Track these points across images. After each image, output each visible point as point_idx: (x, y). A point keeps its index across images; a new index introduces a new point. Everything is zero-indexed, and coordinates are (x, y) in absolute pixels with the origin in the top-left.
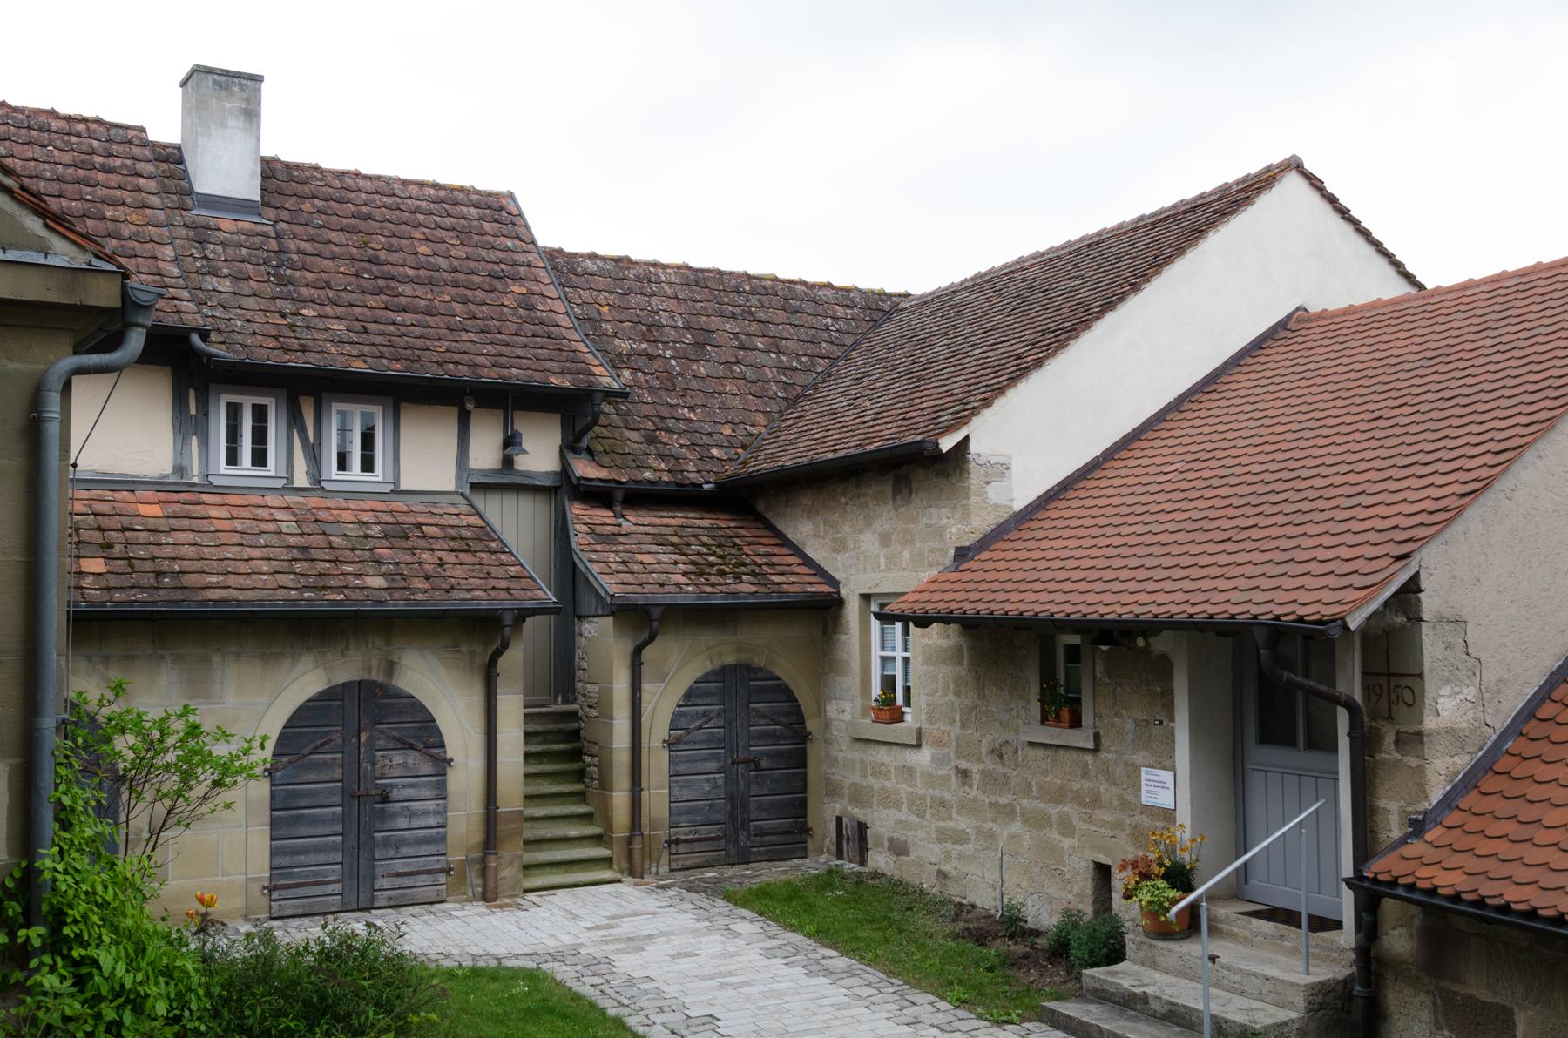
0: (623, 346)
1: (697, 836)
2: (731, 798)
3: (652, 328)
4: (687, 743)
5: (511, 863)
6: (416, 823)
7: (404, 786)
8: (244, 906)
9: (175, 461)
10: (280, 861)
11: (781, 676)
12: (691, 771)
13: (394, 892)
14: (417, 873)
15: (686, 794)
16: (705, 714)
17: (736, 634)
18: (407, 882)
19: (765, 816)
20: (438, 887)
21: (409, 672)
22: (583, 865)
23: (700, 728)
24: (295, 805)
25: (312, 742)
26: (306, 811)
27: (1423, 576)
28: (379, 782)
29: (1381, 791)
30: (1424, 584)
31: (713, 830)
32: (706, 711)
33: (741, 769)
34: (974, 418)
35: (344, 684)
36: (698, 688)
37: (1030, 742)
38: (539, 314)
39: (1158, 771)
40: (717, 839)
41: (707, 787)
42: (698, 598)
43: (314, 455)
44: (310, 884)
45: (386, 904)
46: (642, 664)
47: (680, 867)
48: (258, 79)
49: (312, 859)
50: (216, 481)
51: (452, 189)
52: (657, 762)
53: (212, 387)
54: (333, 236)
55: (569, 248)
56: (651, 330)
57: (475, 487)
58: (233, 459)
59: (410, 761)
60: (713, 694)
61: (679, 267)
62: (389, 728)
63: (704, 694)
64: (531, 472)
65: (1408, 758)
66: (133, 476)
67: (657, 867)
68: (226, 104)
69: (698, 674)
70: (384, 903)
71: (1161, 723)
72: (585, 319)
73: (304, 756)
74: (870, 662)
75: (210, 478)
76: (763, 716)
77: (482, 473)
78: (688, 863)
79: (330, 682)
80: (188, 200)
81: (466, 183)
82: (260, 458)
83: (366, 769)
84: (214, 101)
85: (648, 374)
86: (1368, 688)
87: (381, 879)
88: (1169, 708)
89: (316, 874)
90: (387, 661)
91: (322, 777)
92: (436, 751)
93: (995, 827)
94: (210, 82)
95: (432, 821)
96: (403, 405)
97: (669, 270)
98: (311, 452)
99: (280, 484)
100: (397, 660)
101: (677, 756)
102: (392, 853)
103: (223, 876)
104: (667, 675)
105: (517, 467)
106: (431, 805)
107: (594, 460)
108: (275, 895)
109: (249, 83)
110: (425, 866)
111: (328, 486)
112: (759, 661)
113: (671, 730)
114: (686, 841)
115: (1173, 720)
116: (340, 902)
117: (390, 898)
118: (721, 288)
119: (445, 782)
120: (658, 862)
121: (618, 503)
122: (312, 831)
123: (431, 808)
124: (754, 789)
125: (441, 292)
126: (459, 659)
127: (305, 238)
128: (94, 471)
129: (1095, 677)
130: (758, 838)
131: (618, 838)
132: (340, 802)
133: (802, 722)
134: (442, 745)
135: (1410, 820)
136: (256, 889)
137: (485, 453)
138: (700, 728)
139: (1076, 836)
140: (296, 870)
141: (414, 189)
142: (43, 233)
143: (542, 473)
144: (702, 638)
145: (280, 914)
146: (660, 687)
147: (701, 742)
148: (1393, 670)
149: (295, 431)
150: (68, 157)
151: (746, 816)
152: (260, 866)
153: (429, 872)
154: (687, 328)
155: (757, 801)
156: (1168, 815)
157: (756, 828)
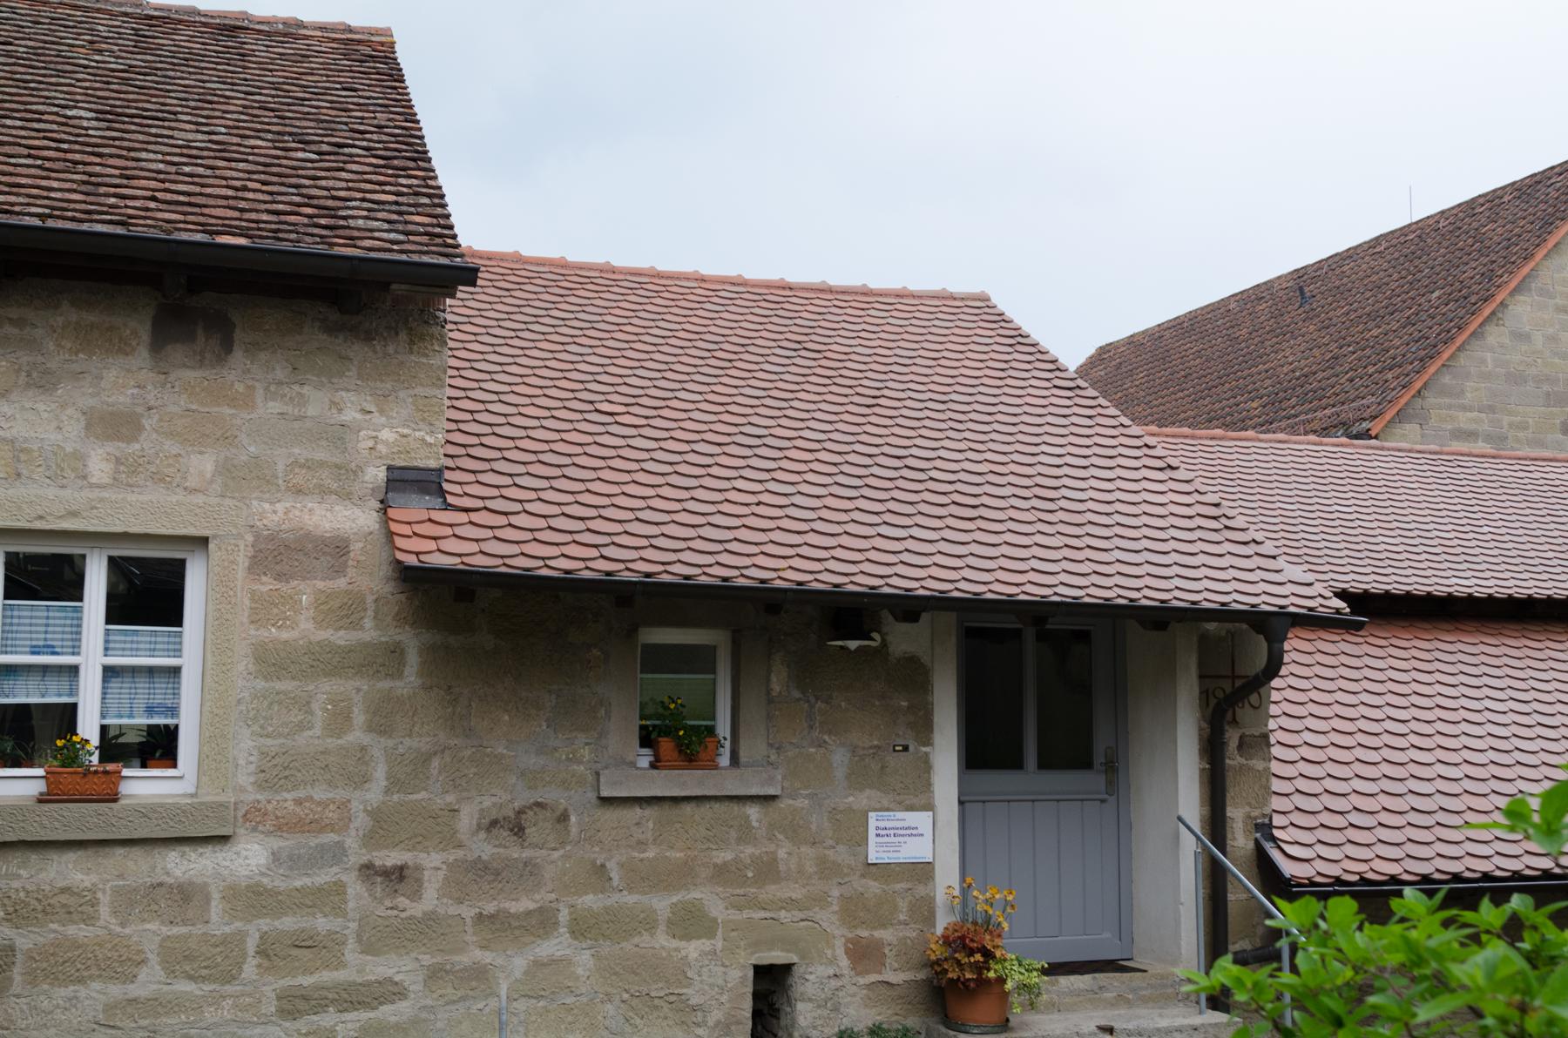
29: (1229, 801)
39: (900, 815)
65: (1254, 762)
71: (906, 748)
86: (1207, 691)
88: (924, 728)
93: (487, 957)
115: (928, 742)
129: (769, 692)
135: (1256, 825)
139: (719, 933)
148: (1238, 672)
156: (923, 872)
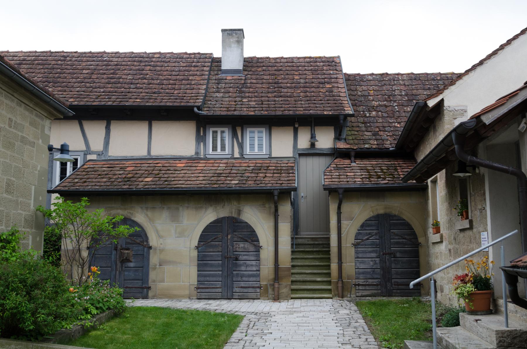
0: (375, 103)
1: (367, 283)
2: (382, 268)
3: (391, 96)
4: (362, 245)
5: (286, 287)
6: (248, 269)
7: (244, 255)
8: (189, 293)
9: (196, 151)
10: (202, 279)
11: (405, 219)
12: (364, 256)
13: (240, 293)
14: (249, 287)
15: (362, 266)
16: (370, 234)
17: (384, 202)
18: (245, 290)
19: (399, 277)
20: (257, 293)
21: (246, 214)
22: (320, 292)
23: (368, 239)
24: (205, 259)
25: (211, 238)
26: (209, 262)
28: (234, 253)
31: (375, 281)
32: (370, 232)
33: (387, 257)
34: (445, 91)
35: (222, 218)
36: (367, 223)
38: (334, 93)
40: (377, 285)
41: (371, 263)
42: (360, 185)
43: (241, 146)
44: (208, 288)
45: (237, 298)
46: (341, 213)
47: (360, 295)
48: (242, 30)
49: (211, 279)
50: (208, 156)
51: (316, 58)
52: (349, 252)
54: (265, 77)
55: (362, 73)
56: (390, 97)
57: (300, 155)
58: (215, 148)
59: (246, 246)
61: (409, 74)
62: (238, 234)
63: (369, 226)
66: (182, 156)
67: (350, 294)
68: (231, 40)
69: (367, 217)
72: (362, 96)
73: (209, 242)
74: (437, 211)
75: (206, 156)
76: (397, 235)
77: (303, 150)
78: (364, 294)
79: (218, 217)
80: (220, 72)
81: (322, 55)
82: (223, 148)
83: (230, 248)
84: (227, 40)
85: (383, 112)
87: (236, 288)
89: (212, 285)
90: (238, 210)
91: (215, 250)
92: (255, 243)
94: (226, 34)
95: (254, 269)
96: (273, 127)
97: (404, 76)
99: (229, 156)
100: (242, 210)
101: (358, 250)
102: (239, 279)
103: (182, 283)
104: (354, 218)
105: (316, 147)
106: (254, 263)
107: (346, 142)
108: (199, 291)
109: (239, 32)
110: (252, 285)
111: (245, 156)
113: (355, 239)
114: (363, 285)
116: (221, 295)
117: (239, 296)
118: (426, 79)
119: (259, 254)
120: (351, 292)
121: (353, 157)
122: (211, 269)
123: (254, 264)
124: (393, 266)
125: (297, 90)
126: (265, 209)
127: (255, 79)
128: (171, 155)
130: (396, 286)
131: (334, 282)
132: (221, 260)
133: (416, 238)
134: (258, 241)
136: (193, 288)
137: (304, 142)
138: (368, 239)
140: (206, 282)
141: (301, 60)
143: (326, 148)
144: (369, 203)
145: (200, 297)
146: (350, 222)
149: (235, 139)
150: (185, 65)
153: (253, 287)
154: (406, 95)
157: (395, 282)
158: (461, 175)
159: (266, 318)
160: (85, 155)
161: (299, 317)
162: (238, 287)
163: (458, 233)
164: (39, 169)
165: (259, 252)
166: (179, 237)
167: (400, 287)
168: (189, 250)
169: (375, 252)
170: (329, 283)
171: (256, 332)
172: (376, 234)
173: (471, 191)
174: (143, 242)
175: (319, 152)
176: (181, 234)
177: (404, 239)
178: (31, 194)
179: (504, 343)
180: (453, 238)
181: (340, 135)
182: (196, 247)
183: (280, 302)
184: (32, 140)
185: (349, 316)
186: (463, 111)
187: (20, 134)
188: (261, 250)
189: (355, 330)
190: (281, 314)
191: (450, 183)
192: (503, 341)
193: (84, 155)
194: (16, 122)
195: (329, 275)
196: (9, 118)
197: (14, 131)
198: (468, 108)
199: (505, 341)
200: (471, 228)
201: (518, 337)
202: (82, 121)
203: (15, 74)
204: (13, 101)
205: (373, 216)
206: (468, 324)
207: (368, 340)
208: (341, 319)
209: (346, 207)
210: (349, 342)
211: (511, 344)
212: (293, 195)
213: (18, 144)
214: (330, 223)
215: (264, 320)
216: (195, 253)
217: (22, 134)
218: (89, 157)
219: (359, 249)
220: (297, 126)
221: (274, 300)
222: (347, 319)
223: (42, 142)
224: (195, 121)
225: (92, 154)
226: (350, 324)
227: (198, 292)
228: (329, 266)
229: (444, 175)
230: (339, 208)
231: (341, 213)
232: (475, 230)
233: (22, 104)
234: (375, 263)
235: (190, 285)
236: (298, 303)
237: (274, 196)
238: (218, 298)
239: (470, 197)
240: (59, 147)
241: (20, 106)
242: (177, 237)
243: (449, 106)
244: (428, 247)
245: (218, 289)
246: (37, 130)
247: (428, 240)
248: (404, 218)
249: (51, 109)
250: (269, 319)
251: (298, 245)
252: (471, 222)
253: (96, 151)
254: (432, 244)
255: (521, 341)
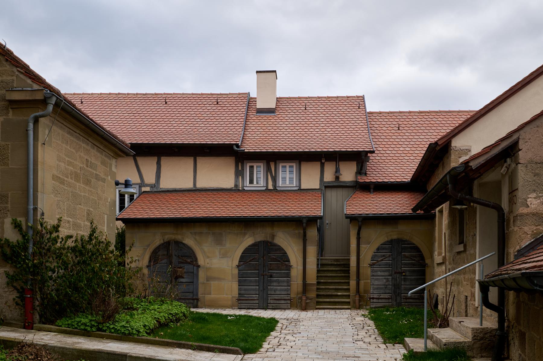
4: (377, 265)
11: (415, 243)
16: (384, 256)
18: (278, 302)
23: (382, 260)
27: (521, 143)
30: (521, 145)
31: (386, 296)
36: (382, 247)
37: (457, 252)
40: (389, 299)
43: (274, 180)
44: (247, 300)
46: (360, 238)
47: (374, 307)
50: (246, 188)
52: (366, 271)
53: (245, 161)
57: (326, 187)
58: (251, 182)
60: (386, 249)
63: (383, 249)
64: (345, 181)
69: (382, 242)
70: (271, 308)
73: (247, 262)
76: (407, 257)
77: (329, 182)
78: (377, 306)
89: (251, 297)
92: (287, 263)
98: (274, 179)
99: (264, 188)
101: (373, 269)
102: (273, 293)
108: (239, 302)
111: (278, 188)
112: (406, 238)
114: (376, 298)
119: (290, 272)
130: (405, 300)
136: (234, 299)
138: (382, 260)
142: (31, 83)
145: (241, 307)
147: (383, 265)
151: (400, 292)
152: (236, 293)
153: (285, 300)
155: (404, 287)
157: (404, 296)
158: (459, 207)
159: (296, 322)
160: (140, 187)
161: (323, 322)
162: (272, 300)
163: (456, 255)
164: (109, 200)
165: (290, 270)
166: (223, 258)
167: (408, 300)
168: (231, 268)
169: (388, 271)
170: (348, 297)
171: (288, 332)
172: (389, 256)
173: (467, 221)
174: (192, 262)
175: (343, 185)
176: (224, 255)
177: (413, 260)
178: (104, 222)
179: (477, 337)
180: (452, 259)
181: (361, 169)
182: (237, 266)
183: (307, 311)
184: (104, 177)
185: (363, 322)
186: (468, 150)
187: (95, 172)
188: (291, 269)
189: (367, 331)
190: (307, 320)
191: (452, 212)
192: (477, 336)
193: (139, 187)
194: (91, 162)
195: (348, 290)
196: (86, 159)
197: (90, 170)
198: (472, 148)
199: (478, 336)
200: (465, 251)
201: (488, 333)
202: (136, 157)
203: (91, 122)
204: (88, 144)
205: (387, 241)
206: (454, 325)
207: (377, 338)
208: (356, 324)
209: (365, 232)
210: (361, 340)
211: (483, 338)
212: (319, 223)
213: (93, 180)
214: (350, 246)
215: (294, 324)
216: (236, 271)
217: (96, 172)
218: (144, 189)
219: (374, 269)
220: (323, 161)
221: (302, 310)
222: (362, 324)
223: (111, 178)
224: (234, 157)
225: (146, 187)
226: (363, 327)
227: (239, 303)
228: (348, 284)
229: (448, 206)
230: (358, 234)
231: (360, 238)
232: (468, 252)
233: (95, 147)
234: (387, 280)
235: (233, 297)
236: (321, 312)
237: (303, 223)
238: (256, 308)
239: (466, 225)
240: (124, 182)
241: (94, 148)
242: (221, 258)
243: (455, 146)
244: (434, 267)
245: (255, 301)
246: (107, 169)
247: (434, 261)
248: (414, 242)
249: (117, 150)
250: (298, 323)
251: (323, 265)
252: (465, 246)
253: (149, 183)
254: (436, 265)
255: (491, 336)
